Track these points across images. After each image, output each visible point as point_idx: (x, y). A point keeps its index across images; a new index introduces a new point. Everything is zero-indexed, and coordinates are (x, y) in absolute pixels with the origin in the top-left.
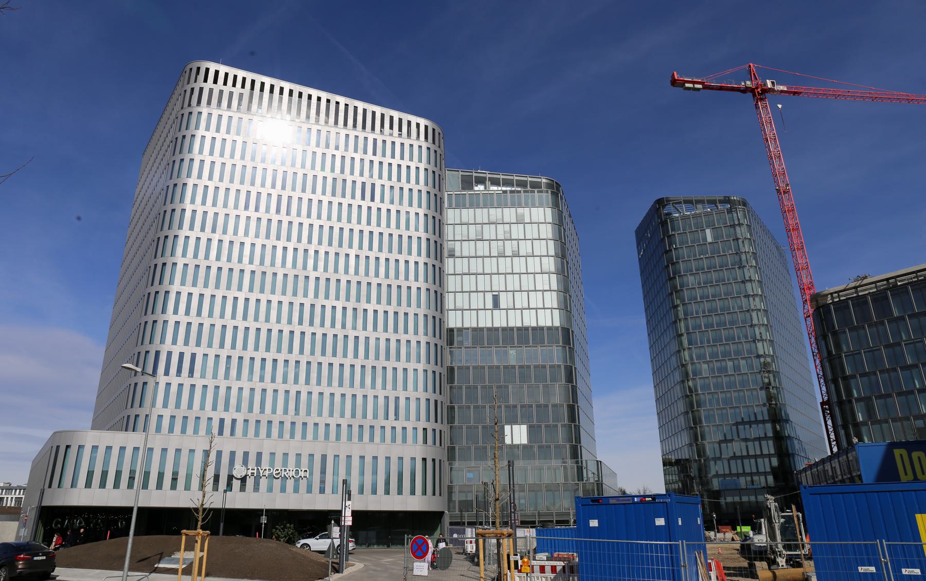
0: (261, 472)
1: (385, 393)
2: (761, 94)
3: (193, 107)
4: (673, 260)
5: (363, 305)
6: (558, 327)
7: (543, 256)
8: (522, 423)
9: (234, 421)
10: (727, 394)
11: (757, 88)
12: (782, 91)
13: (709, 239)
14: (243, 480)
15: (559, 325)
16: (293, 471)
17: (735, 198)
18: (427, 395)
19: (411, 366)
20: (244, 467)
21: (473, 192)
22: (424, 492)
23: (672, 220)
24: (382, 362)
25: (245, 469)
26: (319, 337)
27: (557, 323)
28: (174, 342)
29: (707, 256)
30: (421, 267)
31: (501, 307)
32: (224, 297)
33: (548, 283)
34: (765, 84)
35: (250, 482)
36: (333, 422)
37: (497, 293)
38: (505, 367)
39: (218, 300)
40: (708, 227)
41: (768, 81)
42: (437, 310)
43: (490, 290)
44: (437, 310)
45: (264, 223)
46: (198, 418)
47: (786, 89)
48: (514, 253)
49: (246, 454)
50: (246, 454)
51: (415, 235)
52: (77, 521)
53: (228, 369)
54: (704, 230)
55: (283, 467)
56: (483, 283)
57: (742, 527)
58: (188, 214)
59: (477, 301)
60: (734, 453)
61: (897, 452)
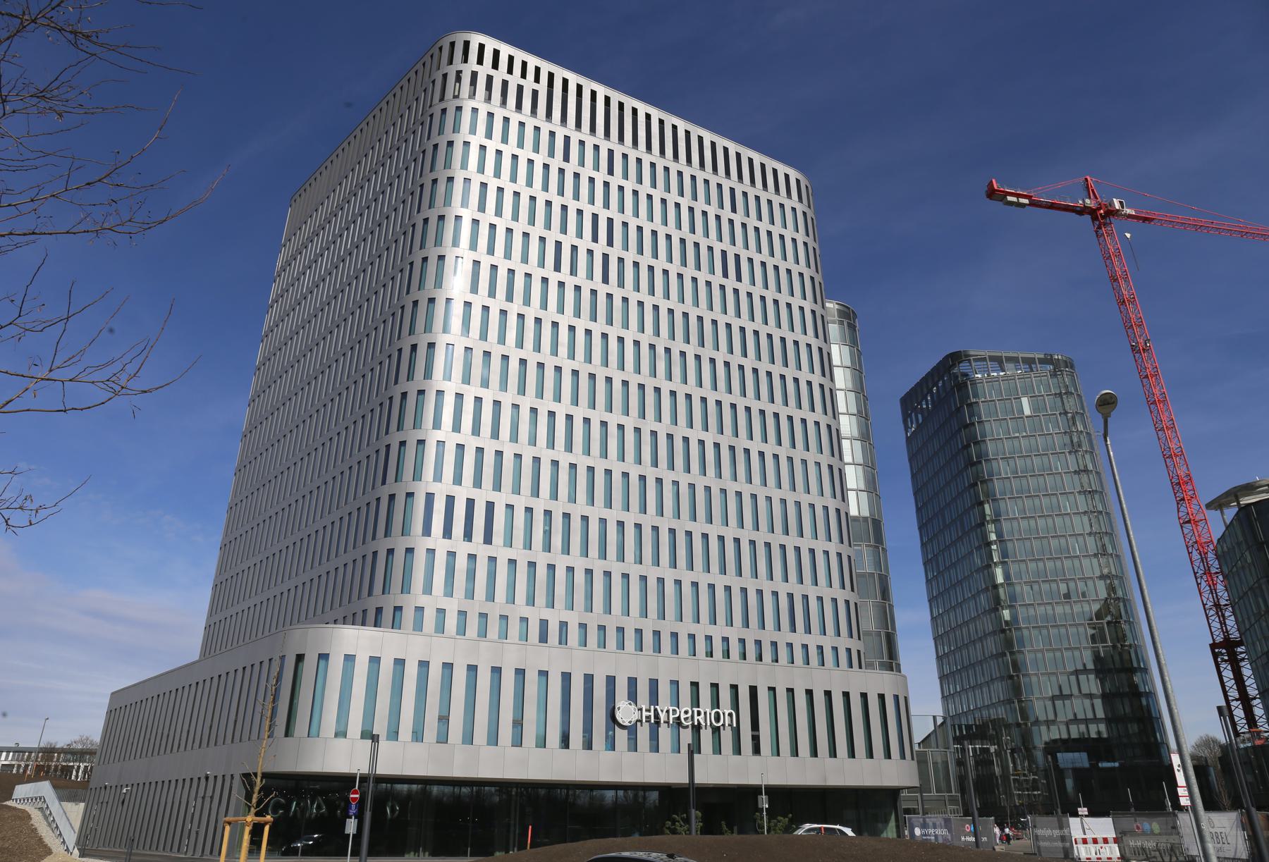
2: (1103, 217)
3: (463, 99)
4: (977, 438)
10: (1061, 630)
11: (1099, 209)
12: (1130, 216)
13: (1027, 411)
14: (632, 730)
17: (1060, 357)
20: (633, 706)
23: (974, 382)
29: (1025, 434)
33: (850, 453)
34: (1112, 204)
35: (643, 733)
40: (1024, 394)
41: (1114, 200)
42: (833, 456)
44: (833, 456)
47: (1134, 213)
49: (633, 682)
50: (633, 682)
52: (312, 804)
53: (548, 534)
54: (1019, 398)
55: (671, 706)
60: (1075, 715)
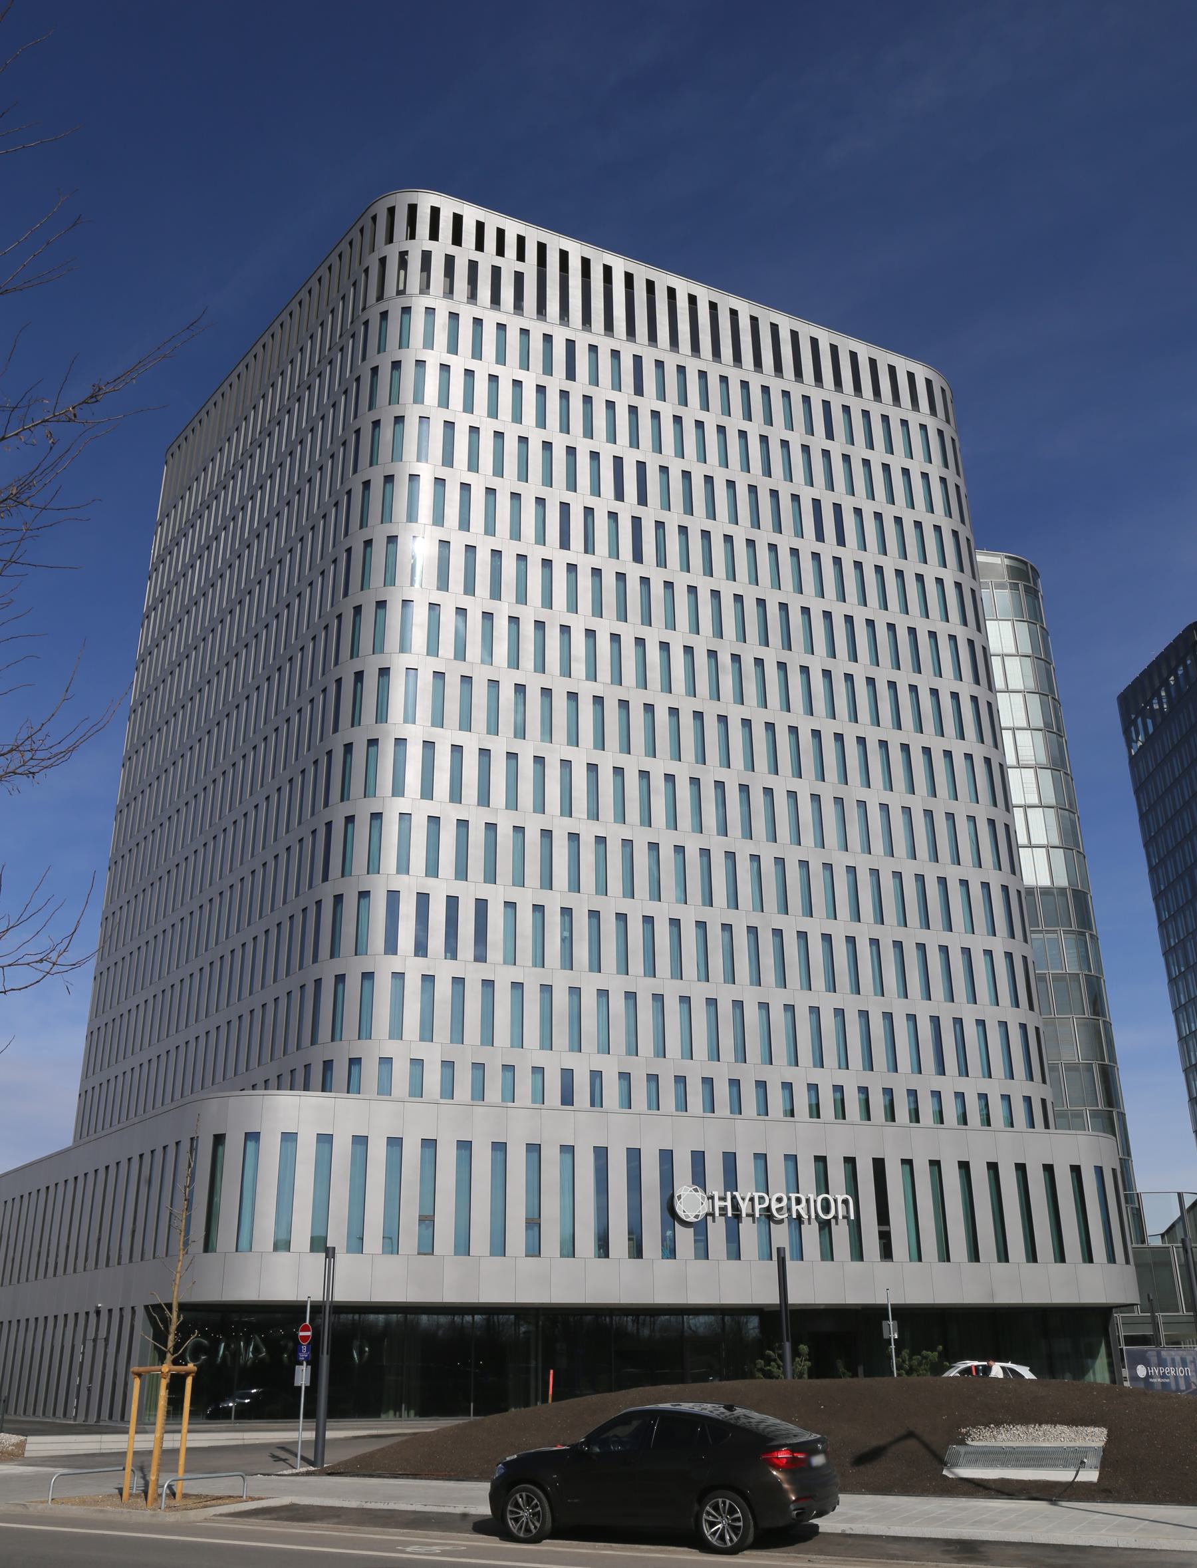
6: (1064, 889)
7: (1019, 729)
15: (1067, 885)
20: (700, 1193)
22: (1112, 1258)
27: (1062, 881)
35: (717, 1232)
49: (698, 1159)
53: (568, 942)
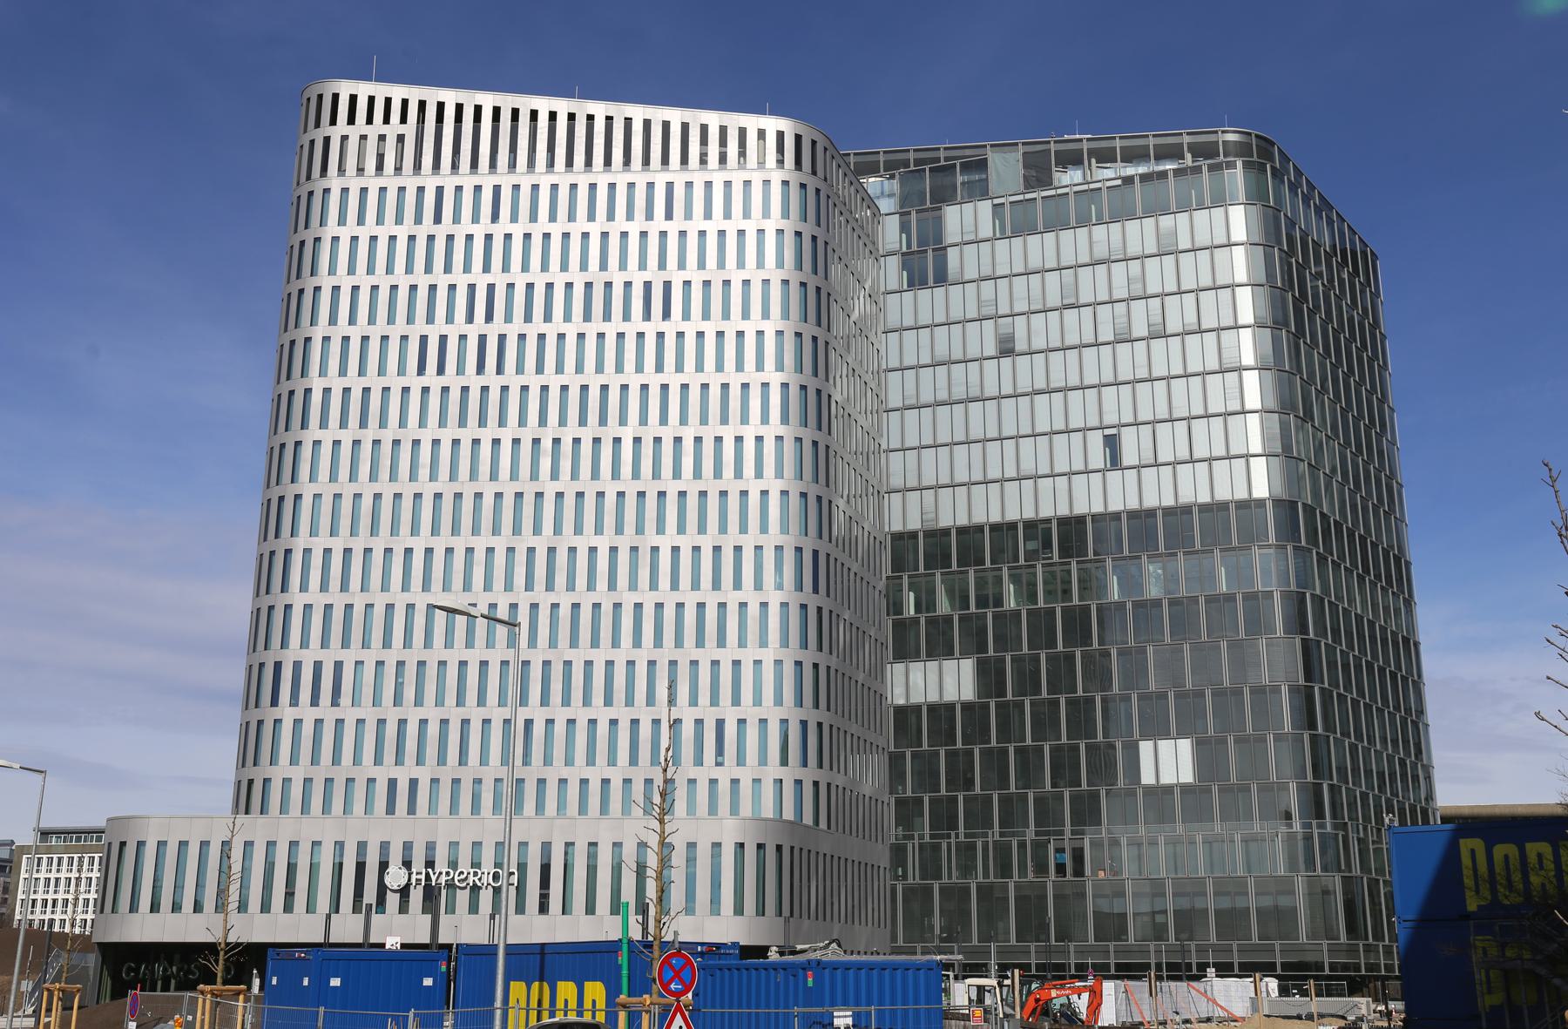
0: (434, 878)
1: (697, 713)
5: (651, 538)
8: (1181, 734)
9: (413, 783)
14: (404, 892)
15: (1268, 496)
16: (489, 874)
18: (801, 714)
19: (747, 656)
21: (1052, 192)
24: (690, 651)
25: (405, 874)
26: (565, 612)
28: (304, 644)
30: (769, 446)
31: (1125, 463)
32: (698, 440)
36: (594, 776)
37: (1113, 431)
38: (1137, 605)
39: (688, 445)
43: (1098, 425)
45: (455, 395)
46: (350, 781)
48: (1117, 337)
51: (755, 379)
56: (1080, 409)
57: (558, 1007)
58: (317, 397)
59: (1067, 453)
61: (1466, 845)
